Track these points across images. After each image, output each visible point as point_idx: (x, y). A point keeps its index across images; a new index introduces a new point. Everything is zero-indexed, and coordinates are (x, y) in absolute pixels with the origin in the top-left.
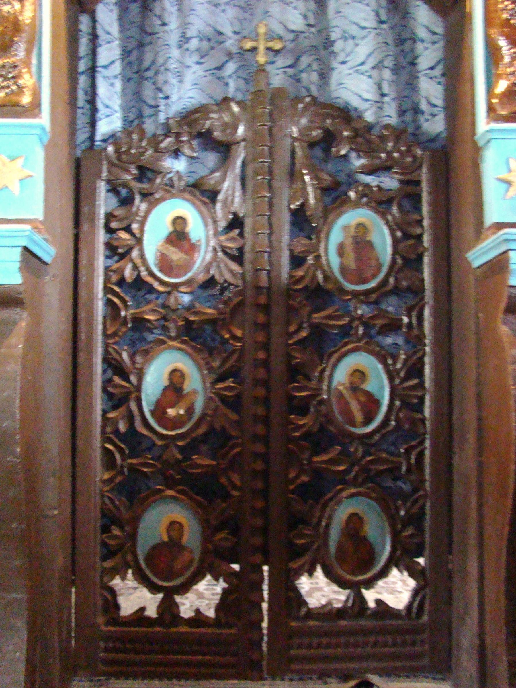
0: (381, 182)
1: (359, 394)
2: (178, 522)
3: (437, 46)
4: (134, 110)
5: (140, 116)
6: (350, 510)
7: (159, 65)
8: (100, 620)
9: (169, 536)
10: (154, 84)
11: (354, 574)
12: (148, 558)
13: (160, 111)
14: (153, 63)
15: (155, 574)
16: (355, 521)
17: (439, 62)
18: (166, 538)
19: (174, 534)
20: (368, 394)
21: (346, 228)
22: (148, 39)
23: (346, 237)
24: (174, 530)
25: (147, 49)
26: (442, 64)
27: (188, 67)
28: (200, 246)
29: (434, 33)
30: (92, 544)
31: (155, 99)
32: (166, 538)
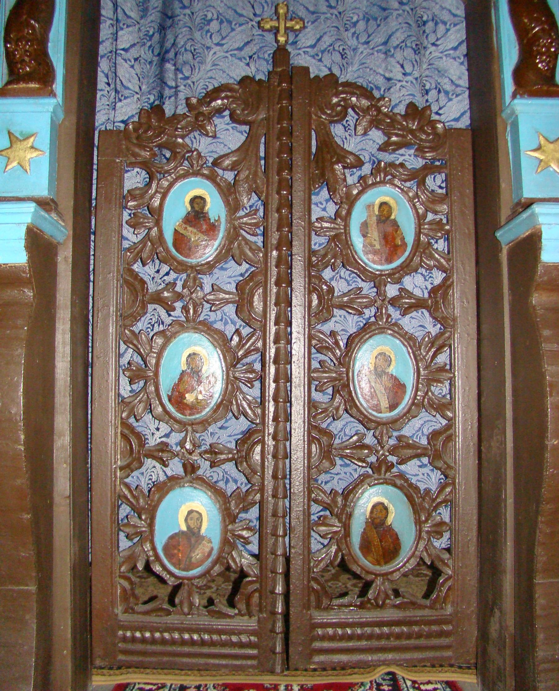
0: (406, 161)
1: (385, 378)
2: (197, 512)
3: (458, 27)
4: (155, 92)
5: (161, 97)
6: (376, 499)
7: (179, 46)
8: (119, 610)
9: (188, 527)
10: (175, 65)
11: (378, 563)
12: (166, 548)
13: (179, 91)
14: (174, 44)
15: (174, 565)
16: (380, 510)
17: (460, 43)
18: (184, 528)
19: (192, 524)
20: (395, 379)
21: (369, 207)
22: (169, 22)
23: (369, 216)
24: (191, 519)
25: (168, 31)
26: (465, 44)
27: (208, 48)
28: (219, 226)
29: (455, 16)
30: (109, 533)
31: (176, 80)
32: (184, 528)
